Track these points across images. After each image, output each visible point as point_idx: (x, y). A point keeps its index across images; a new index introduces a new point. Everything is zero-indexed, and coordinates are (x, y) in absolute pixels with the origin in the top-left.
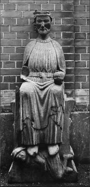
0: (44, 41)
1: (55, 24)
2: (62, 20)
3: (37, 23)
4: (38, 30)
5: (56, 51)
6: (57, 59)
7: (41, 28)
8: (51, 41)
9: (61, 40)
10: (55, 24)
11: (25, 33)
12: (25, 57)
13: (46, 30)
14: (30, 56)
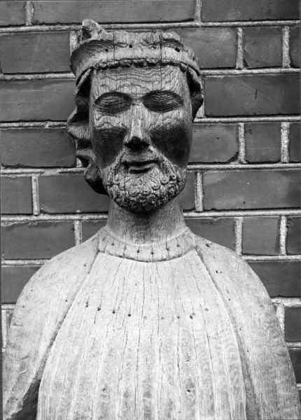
0: (146, 248)
1: (246, 65)
2: (286, 36)
3: (99, 119)
4: (107, 173)
5: (234, 320)
6: (247, 376)
7: (124, 155)
8: (196, 248)
9: (284, 172)
10: (240, 64)
11: (51, 130)
12: (17, 366)
13: (164, 170)
14: (44, 362)
